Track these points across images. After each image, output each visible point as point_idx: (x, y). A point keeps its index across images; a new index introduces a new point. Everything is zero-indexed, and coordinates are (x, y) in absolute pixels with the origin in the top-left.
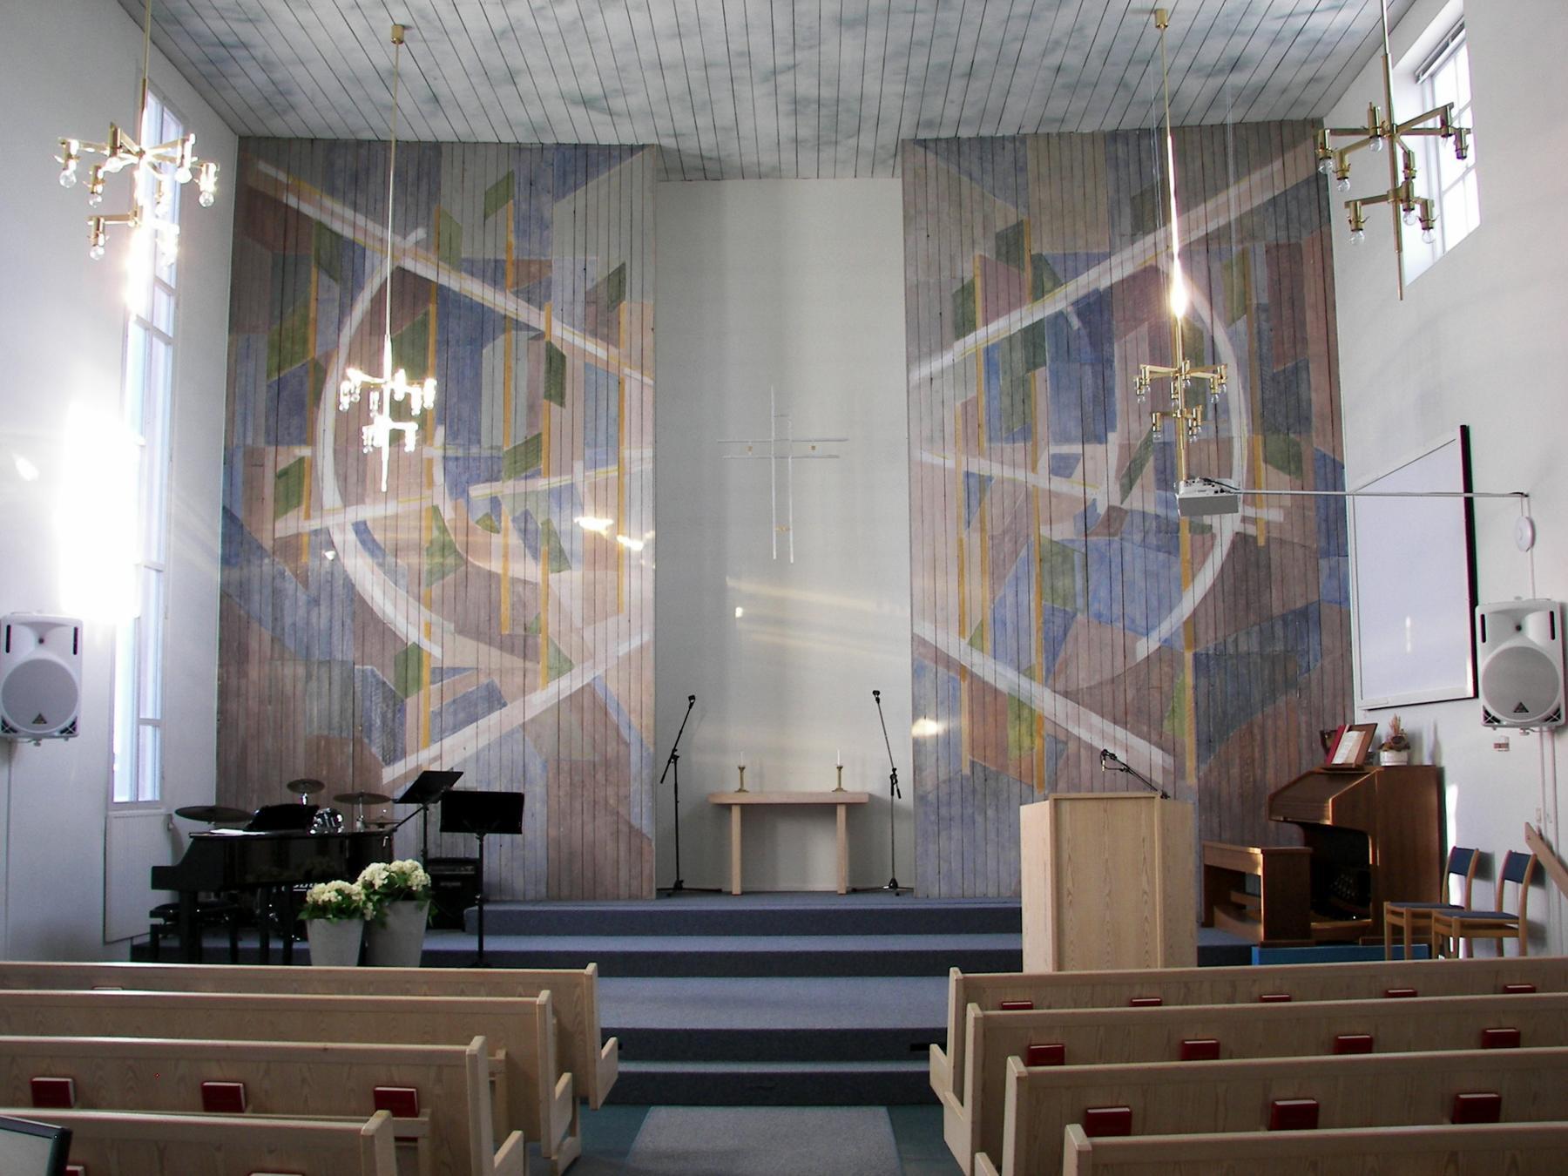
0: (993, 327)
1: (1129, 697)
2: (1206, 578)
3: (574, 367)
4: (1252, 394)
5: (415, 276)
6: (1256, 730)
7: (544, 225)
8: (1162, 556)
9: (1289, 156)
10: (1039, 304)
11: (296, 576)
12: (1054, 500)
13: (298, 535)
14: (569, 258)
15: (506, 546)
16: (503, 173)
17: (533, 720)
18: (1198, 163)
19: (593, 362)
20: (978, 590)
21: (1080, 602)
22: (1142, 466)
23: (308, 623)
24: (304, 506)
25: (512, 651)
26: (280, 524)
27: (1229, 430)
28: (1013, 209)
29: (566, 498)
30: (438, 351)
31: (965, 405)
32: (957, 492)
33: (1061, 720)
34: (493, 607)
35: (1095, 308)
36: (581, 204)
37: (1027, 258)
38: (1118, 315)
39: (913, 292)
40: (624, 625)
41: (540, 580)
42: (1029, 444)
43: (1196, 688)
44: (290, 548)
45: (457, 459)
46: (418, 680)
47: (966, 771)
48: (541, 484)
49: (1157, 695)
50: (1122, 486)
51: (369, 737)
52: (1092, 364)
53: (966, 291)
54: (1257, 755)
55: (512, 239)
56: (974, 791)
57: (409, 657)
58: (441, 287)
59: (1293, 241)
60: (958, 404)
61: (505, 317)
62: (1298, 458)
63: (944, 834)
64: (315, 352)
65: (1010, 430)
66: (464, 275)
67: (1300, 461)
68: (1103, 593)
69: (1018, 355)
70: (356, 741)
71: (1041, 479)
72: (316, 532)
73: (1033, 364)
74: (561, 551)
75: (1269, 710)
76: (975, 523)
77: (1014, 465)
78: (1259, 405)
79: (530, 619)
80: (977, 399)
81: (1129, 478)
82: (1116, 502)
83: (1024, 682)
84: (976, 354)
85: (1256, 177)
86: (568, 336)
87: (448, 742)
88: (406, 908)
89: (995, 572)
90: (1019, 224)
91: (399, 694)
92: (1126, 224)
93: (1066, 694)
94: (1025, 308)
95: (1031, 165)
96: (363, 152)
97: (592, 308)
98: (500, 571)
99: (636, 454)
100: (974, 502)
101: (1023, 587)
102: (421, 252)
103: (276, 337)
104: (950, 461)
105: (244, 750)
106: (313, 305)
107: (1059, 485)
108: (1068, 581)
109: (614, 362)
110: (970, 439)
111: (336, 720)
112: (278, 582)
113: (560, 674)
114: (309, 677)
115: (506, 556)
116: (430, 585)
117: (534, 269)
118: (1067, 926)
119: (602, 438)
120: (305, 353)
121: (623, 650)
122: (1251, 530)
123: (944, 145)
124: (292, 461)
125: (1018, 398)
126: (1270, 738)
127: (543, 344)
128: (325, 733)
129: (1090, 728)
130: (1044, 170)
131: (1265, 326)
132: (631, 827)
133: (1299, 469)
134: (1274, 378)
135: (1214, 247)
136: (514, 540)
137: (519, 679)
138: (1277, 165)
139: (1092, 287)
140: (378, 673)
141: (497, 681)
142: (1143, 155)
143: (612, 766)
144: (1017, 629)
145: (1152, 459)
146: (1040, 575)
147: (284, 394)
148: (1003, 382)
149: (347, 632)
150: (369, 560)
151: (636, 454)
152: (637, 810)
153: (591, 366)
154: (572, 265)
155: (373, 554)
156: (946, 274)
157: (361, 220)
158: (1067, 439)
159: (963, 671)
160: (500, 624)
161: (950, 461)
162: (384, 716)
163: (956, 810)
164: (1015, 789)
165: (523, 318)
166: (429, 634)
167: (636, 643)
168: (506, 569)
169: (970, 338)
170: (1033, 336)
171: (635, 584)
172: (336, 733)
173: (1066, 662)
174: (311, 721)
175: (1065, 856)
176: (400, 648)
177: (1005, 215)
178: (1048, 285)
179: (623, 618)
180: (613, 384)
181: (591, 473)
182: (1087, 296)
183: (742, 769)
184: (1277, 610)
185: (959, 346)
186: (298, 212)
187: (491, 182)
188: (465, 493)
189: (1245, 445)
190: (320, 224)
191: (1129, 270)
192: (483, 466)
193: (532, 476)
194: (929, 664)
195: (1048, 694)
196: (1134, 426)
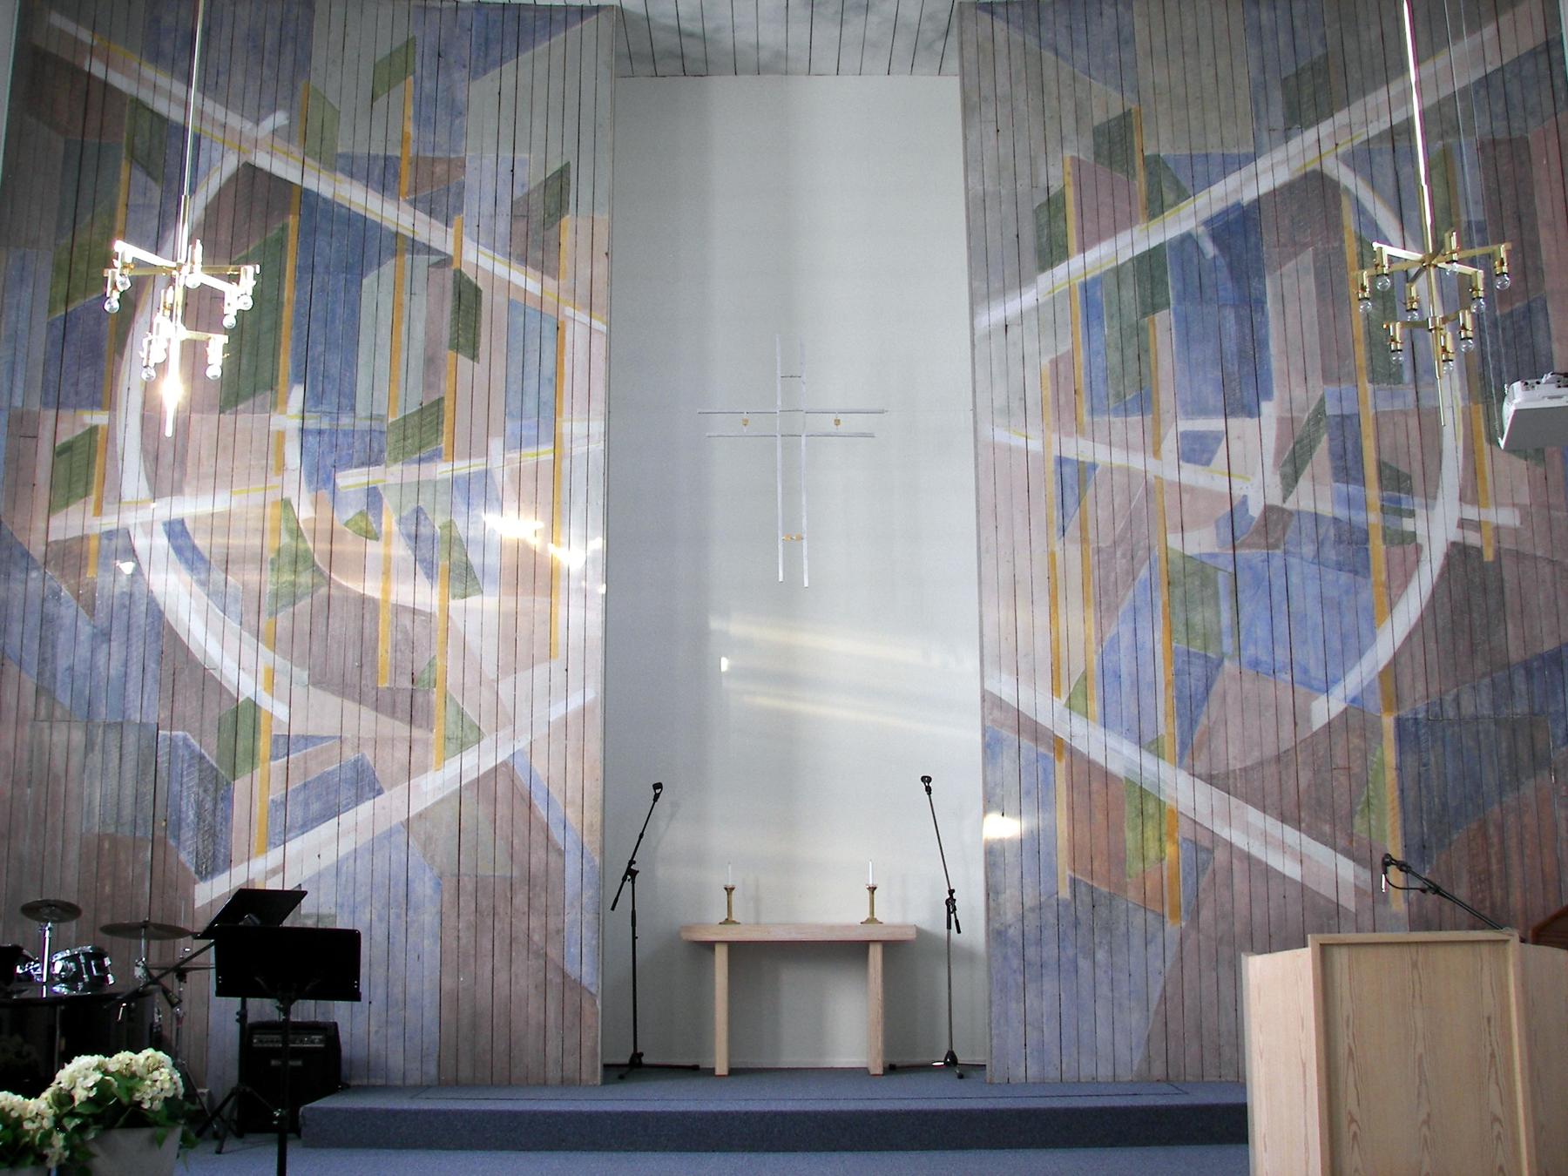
0: (1092, 255)
1: (1303, 785)
3: (493, 307)
5: (271, 176)
6: (1492, 830)
7: (457, 111)
8: (1344, 578)
10: (1156, 223)
11: (78, 597)
12: (1186, 498)
13: (83, 539)
15: (388, 559)
16: (399, 41)
17: (420, 815)
18: (1375, 32)
20: (1078, 623)
21: (1228, 644)
22: (1312, 449)
23: (92, 667)
24: (93, 497)
25: (393, 715)
26: (57, 522)
27: (1436, 397)
28: (1116, 95)
29: (476, 490)
30: (298, 282)
31: (1055, 363)
34: (366, 647)
35: (1238, 229)
36: (508, 80)
37: (1138, 161)
38: (1269, 238)
39: (977, 206)
40: (558, 678)
41: (436, 610)
42: (1148, 418)
43: (1399, 768)
44: (71, 556)
47: (1065, 893)
49: (1343, 779)
50: (1284, 477)
51: (178, 838)
52: (1234, 306)
53: (1053, 206)
54: (1495, 867)
55: (410, 128)
56: (1076, 924)
57: (240, 720)
58: (305, 193)
59: (1516, 134)
60: (1046, 361)
63: (1032, 989)
65: (1120, 397)
66: (340, 176)
68: (1261, 631)
69: (1129, 294)
71: (1167, 467)
72: (110, 534)
73: (1151, 306)
74: (468, 567)
75: (1509, 799)
76: (1073, 529)
79: (421, 665)
80: (1072, 355)
81: (1293, 466)
82: (1275, 498)
83: (1149, 762)
86: (485, 262)
87: (294, 846)
88: (131, 1141)
89: (1102, 600)
90: (1126, 115)
93: (1210, 779)
94: (1137, 229)
95: (1141, 37)
97: (521, 226)
98: (378, 595)
99: (579, 428)
100: (1070, 500)
101: (1144, 623)
102: (280, 143)
103: (65, 256)
104: (1037, 441)
107: (1192, 475)
108: (1209, 613)
109: (550, 299)
111: (127, 812)
113: (462, 747)
114: (89, 746)
116: (274, 613)
117: (440, 169)
119: (531, 404)
121: (557, 712)
122: (1473, 538)
124: (79, 431)
125: (1131, 353)
126: (1513, 843)
127: (449, 273)
128: (112, 829)
129: (1247, 828)
130: (1158, 41)
132: (564, 975)
136: (400, 550)
137: (401, 753)
138: (1489, 31)
139: (1231, 201)
140: (194, 742)
141: (369, 757)
143: (536, 885)
144: (1137, 683)
145: (1325, 438)
146: (1169, 604)
148: (1108, 330)
150: (186, 577)
151: (579, 428)
152: (575, 950)
153: (517, 304)
154: (490, 169)
155: (192, 568)
156: (1023, 184)
159: (1060, 746)
161: (1037, 441)
162: (199, 805)
163: (1050, 951)
164: (1138, 920)
165: (422, 236)
166: (271, 686)
167: (575, 702)
168: (386, 591)
169: (1060, 271)
170: (1150, 265)
171: (576, 614)
173: (1209, 732)
176: (228, 707)
177: (1106, 103)
178: (1169, 197)
179: (557, 665)
182: (1226, 212)
183: (729, 890)
184: (1515, 654)
185: (1044, 280)
186: (106, 85)
187: (383, 51)
188: (330, 481)
189: (1459, 415)
191: (1283, 176)
193: (430, 459)
194: (1009, 735)
195: (1183, 778)
196: (1299, 393)
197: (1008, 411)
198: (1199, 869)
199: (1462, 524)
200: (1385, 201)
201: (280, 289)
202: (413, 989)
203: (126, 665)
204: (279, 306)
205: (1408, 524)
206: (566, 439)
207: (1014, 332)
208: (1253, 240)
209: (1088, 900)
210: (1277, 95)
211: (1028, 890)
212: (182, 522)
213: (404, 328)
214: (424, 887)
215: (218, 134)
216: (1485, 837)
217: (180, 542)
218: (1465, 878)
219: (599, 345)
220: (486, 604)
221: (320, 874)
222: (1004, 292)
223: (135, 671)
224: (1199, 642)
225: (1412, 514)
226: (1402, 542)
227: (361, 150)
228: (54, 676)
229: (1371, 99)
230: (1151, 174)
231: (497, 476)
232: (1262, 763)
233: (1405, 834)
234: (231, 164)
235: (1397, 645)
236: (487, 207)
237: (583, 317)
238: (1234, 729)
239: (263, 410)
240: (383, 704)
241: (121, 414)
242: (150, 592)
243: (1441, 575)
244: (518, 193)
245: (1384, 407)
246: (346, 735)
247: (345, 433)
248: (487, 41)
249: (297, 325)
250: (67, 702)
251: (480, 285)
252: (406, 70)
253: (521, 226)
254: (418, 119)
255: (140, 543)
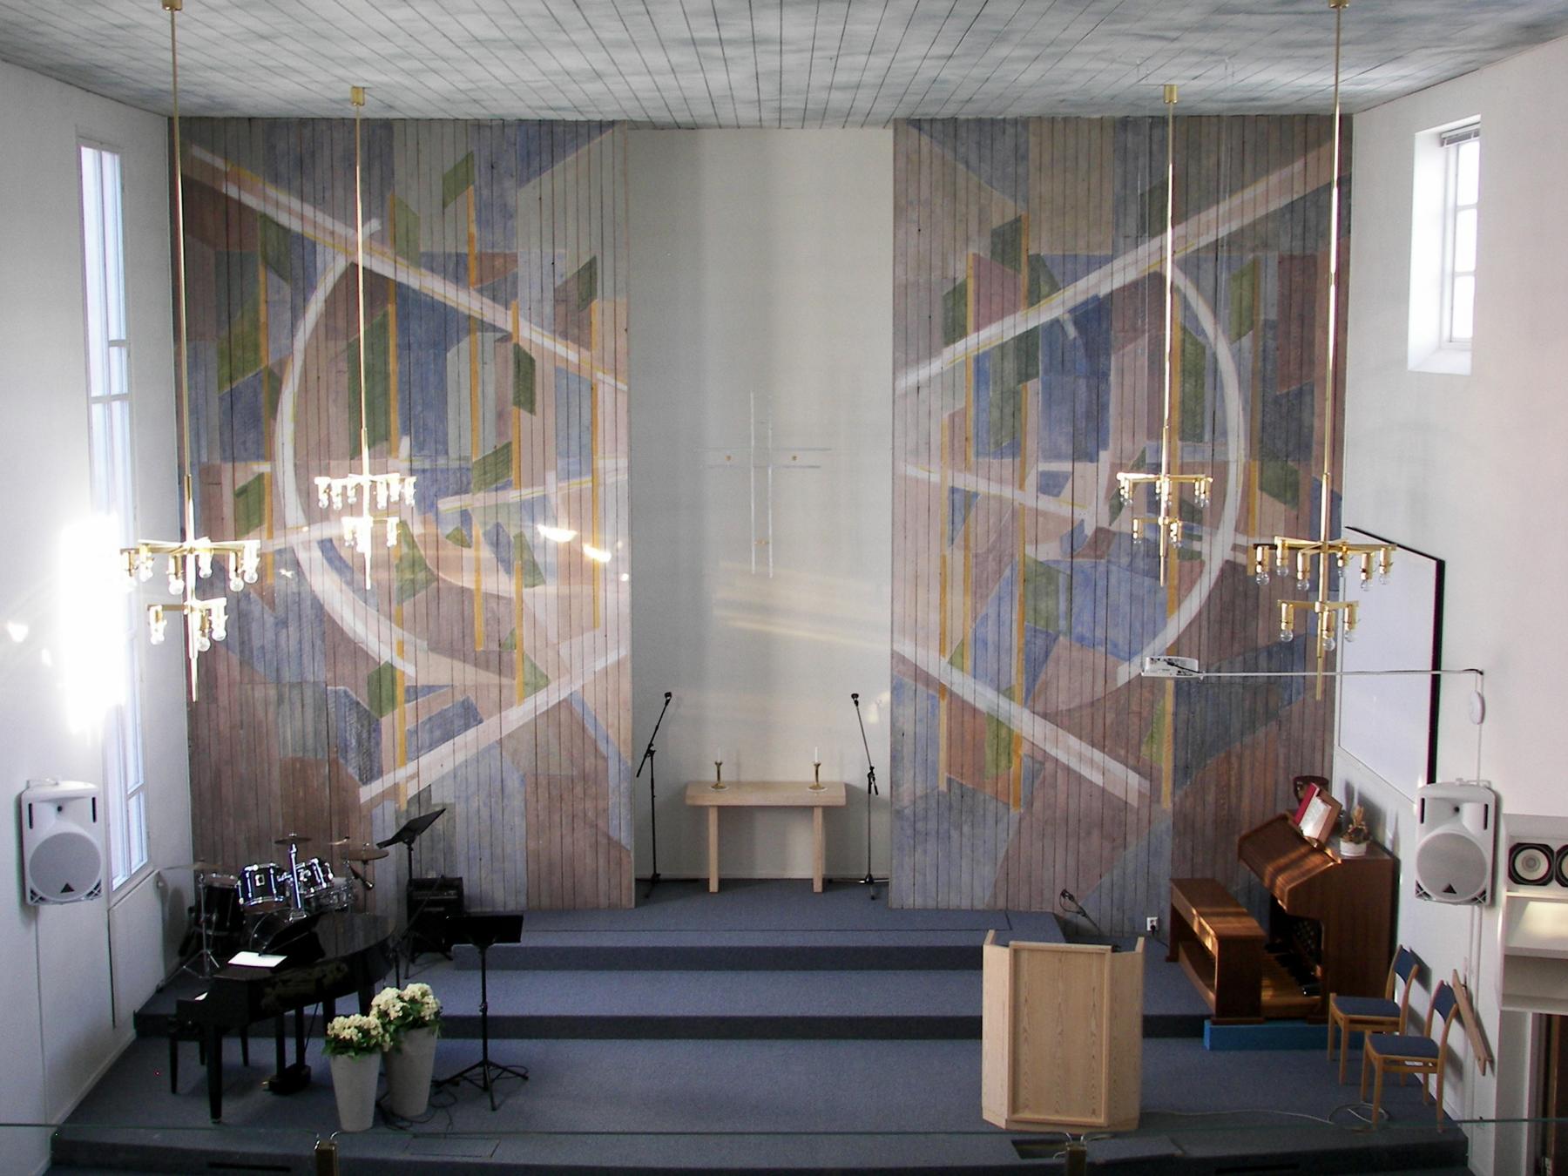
0: (985, 333)
1: (1108, 721)
2: (1193, 604)
4: (1252, 417)
6: (1234, 759)
7: (508, 214)
9: (1312, 156)
10: (1032, 311)
11: (262, 597)
12: (1040, 519)
14: (536, 250)
15: (478, 560)
16: (461, 156)
17: (509, 735)
18: (1213, 160)
19: (562, 366)
20: (959, 601)
21: (1063, 624)
23: (277, 646)
24: (266, 525)
25: (487, 668)
26: (347, 1124)
27: (1226, 453)
28: (1011, 203)
29: (536, 509)
30: (399, 357)
31: (952, 417)
32: (942, 510)
33: (1039, 742)
34: (466, 621)
35: (1093, 316)
37: (1024, 259)
38: (1117, 325)
39: (901, 292)
40: (600, 640)
41: (514, 595)
42: (1018, 460)
43: (1175, 714)
45: (424, 471)
46: (393, 700)
47: (943, 787)
48: (513, 496)
49: (1136, 720)
50: (1111, 507)
51: (346, 759)
52: (1088, 378)
54: (1233, 784)
55: (474, 229)
56: (950, 808)
57: (382, 680)
58: (399, 285)
59: (1308, 252)
60: (946, 415)
61: (470, 317)
62: (1295, 487)
63: (919, 850)
64: (269, 360)
65: (998, 444)
67: (1297, 490)
68: (1087, 617)
69: (1010, 366)
70: (333, 763)
71: (1029, 497)
72: (280, 551)
73: (1025, 376)
74: (534, 564)
75: (1248, 740)
76: (959, 540)
77: (1001, 481)
78: (1258, 425)
79: (505, 634)
80: (965, 411)
82: (1104, 524)
83: (1004, 703)
84: (966, 363)
85: (1274, 179)
86: (536, 338)
89: (977, 588)
90: (1017, 220)
91: (374, 714)
92: (1131, 224)
93: (1045, 716)
94: (1019, 315)
95: (1033, 154)
96: (307, 132)
97: (562, 309)
99: (610, 464)
100: (958, 518)
101: (1005, 608)
102: (376, 246)
103: (225, 344)
104: (936, 475)
105: (218, 774)
106: (263, 307)
107: (1046, 503)
108: (1051, 603)
109: (586, 366)
110: (956, 454)
111: (310, 742)
112: (243, 605)
113: (536, 689)
114: (280, 700)
115: (478, 571)
116: (401, 602)
117: (498, 263)
118: (1023, 1058)
119: (574, 448)
120: (257, 362)
123: (939, 126)
124: (251, 478)
125: (1008, 410)
126: (1247, 767)
127: (510, 346)
129: (1068, 750)
130: (1047, 158)
131: (1271, 344)
132: (609, 838)
133: (1295, 497)
134: (1276, 401)
135: (1223, 254)
136: (486, 553)
137: (494, 694)
138: (1298, 166)
140: (352, 693)
141: (473, 699)
142: (1155, 147)
143: (590, 780)
144: (998, 648)
146: (1024, 595)
147: (238, 406)
148: (993, 393)
149: (318, 654)
150: (335, 576)
151: (610, 464)
152: (616, 822)
153: (562, 371)
154: (540, 262)
155: (339, 571)
156: (937, 274)
157: (309, 210)
158: (1058, 457)
159: (943, 690)
160: (474, 641)
161: (936, 475)
162: (359, 736)
163: (932, 825)
164: (991, 806)
165: (488, 318)
166: (401, 652)
167: (612, 658)
168: (478, 582)
169: (960, 346)
170: (1026, 344)
171: (611, 596)
172: (310, 755)
173: (1046, 684)
174: (285, 744)
175: (1022, 999)
176: (373, 668)
177: (1002, 210)
178: (1045, 289)
179: (599, 633)
180: (585, 389)
181: (564, 484)
182: (1086, 303)
183: (718, 765)
184: (1262, 641)
185: (948, 353)
186: (239, 203)
187: (449, 166)
189: (1241, 468)
190: (264, 217)
191: (1131, 276)
192: (452, 479)
193: (504, 488)
195: (1026, 715)
196: (1128, 445)
197: (917, 452)
198: (1034, 775)
199: (1235, 547)
200: (1206, 301)
201: (386, 363)
202: (508, 850)
203: (300, 642)
204: (386, 377)
205: (1196, 546)
206: (601, 472)
207: (924, 392)
208: (1104, 326)
209: (958, 792)
210: (1134, 209)
211: (919, 785)
212: (331, 540)
213: (480, 389)
214: (513, 783)
215: (329, 240)
216: (1229, 763)
217: (331, 554)
218: (1213, 788)
219: (622, 400)
220: (550, 589)
221: (443, 777)
222: (918, 361)
223: (307, 647)
224: (1042, 623)
225: (1200, 538)
226: (1191, 559)
227: (438, 249)
228: (251, 652)
229: (1204, 216)
230: (1033, 269)
231: (553, 500)
232: (1080, 707)
233: (1175, 757)
234: (341, 265)
235: (1175, 616)
236: (536, 294)
237: (610, 380)
238: (1063, 683)
239: (381, 456)
240: (481, 662)
241: (279, 462)
242: (312, 592)
243: (1216, 583)
244: (559, 282)
245: (1188, 459)
246: (456, 683)
247: (442, 471)
248: (528, 154)
249: (400, 390)
250: (262, 670)
251: (533, 355)
252: (468, 182)
253: (562, 309)
254: (479, 221)
255: (302, 556)
